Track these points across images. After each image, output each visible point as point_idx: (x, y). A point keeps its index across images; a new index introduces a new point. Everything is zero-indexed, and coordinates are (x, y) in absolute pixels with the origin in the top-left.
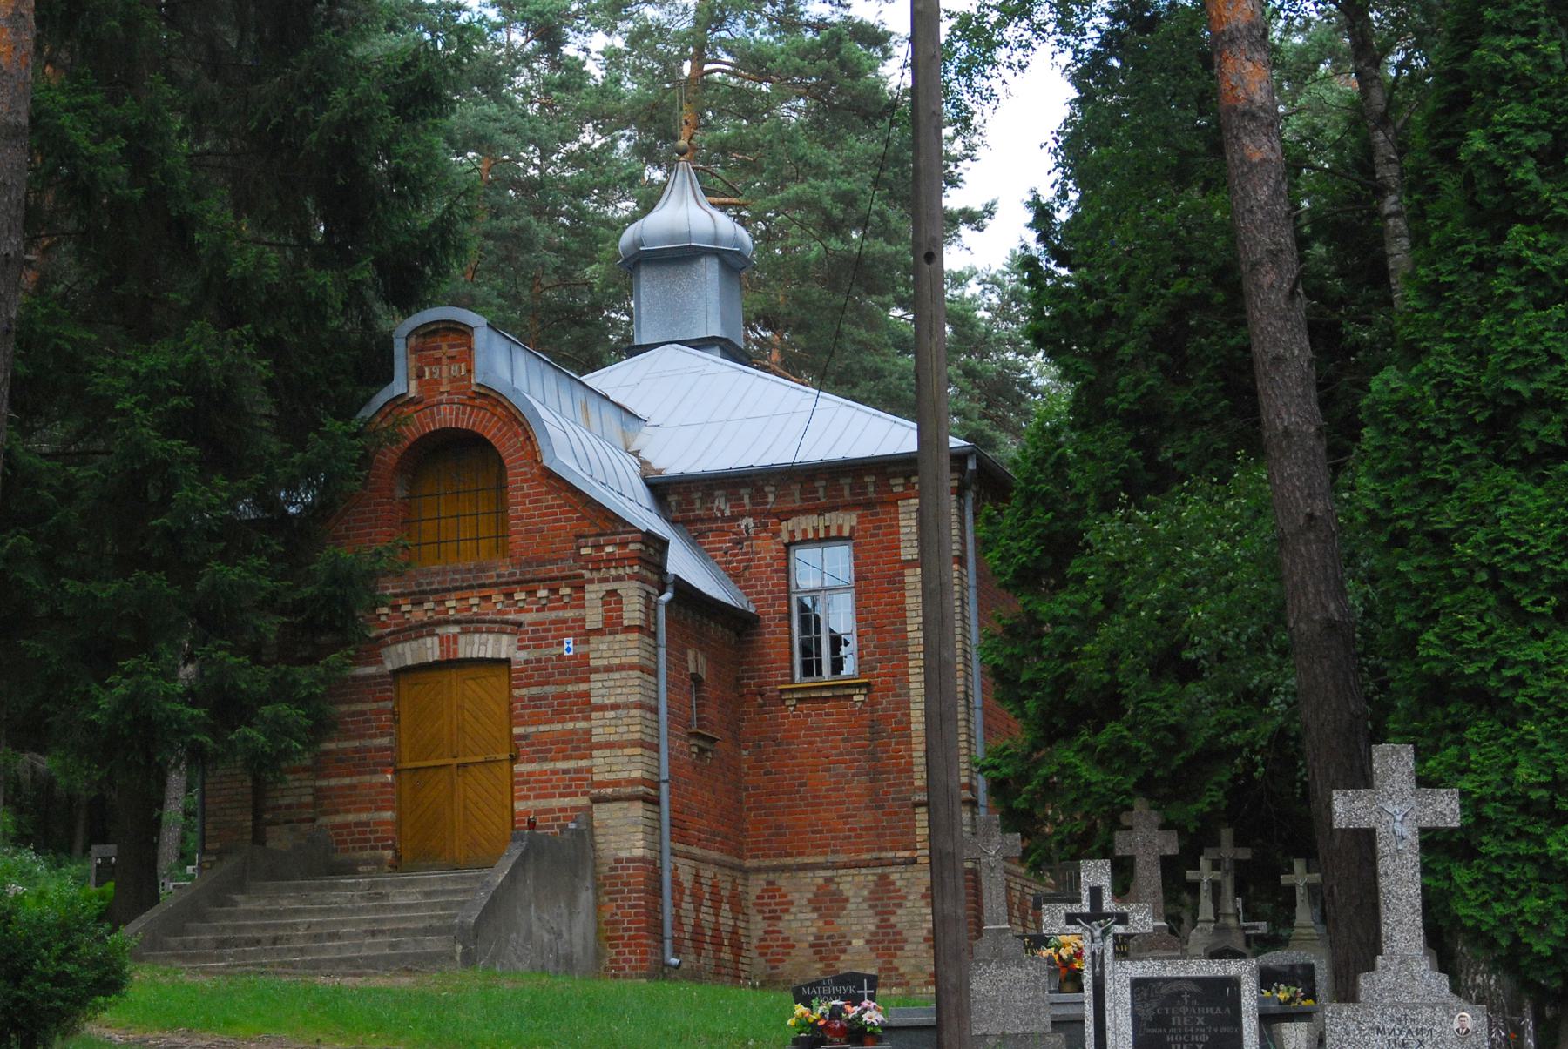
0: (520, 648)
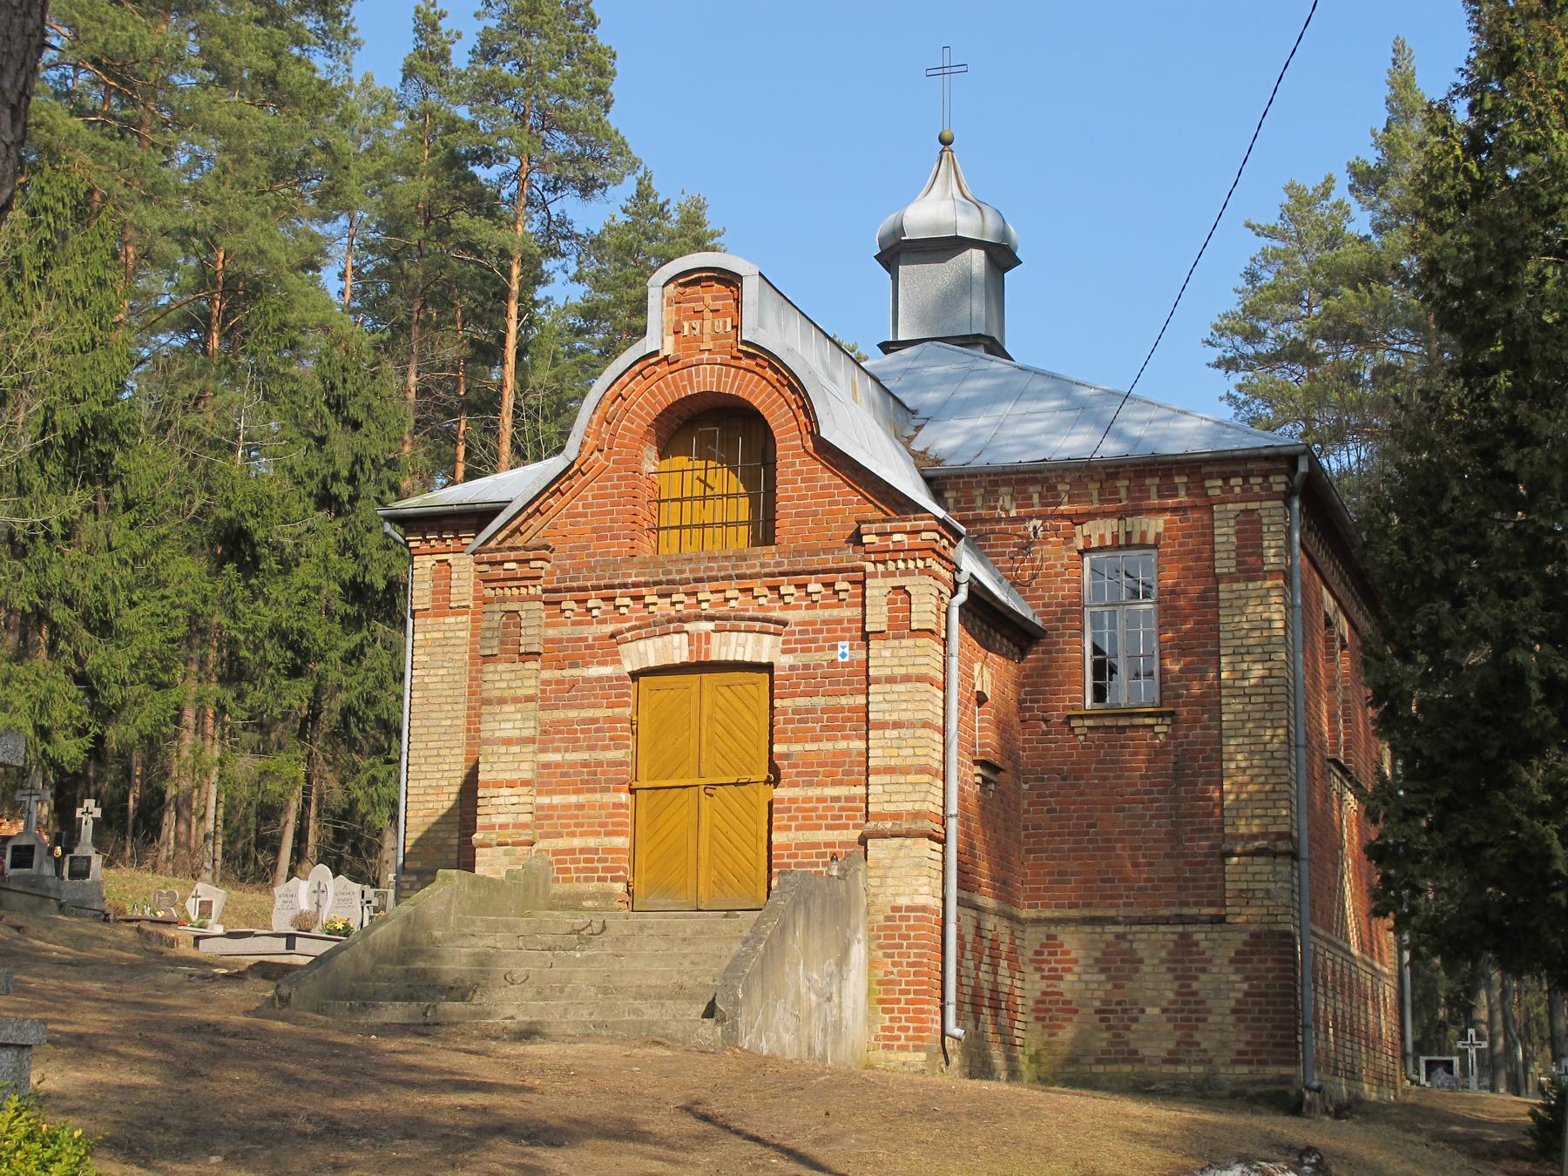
0: (784, 652)
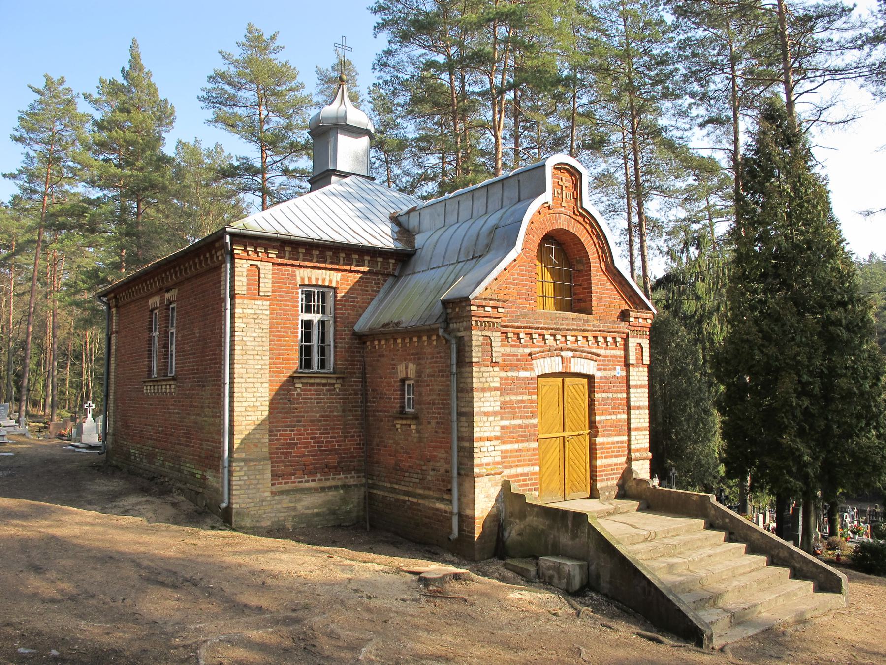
0: (599, 370)
